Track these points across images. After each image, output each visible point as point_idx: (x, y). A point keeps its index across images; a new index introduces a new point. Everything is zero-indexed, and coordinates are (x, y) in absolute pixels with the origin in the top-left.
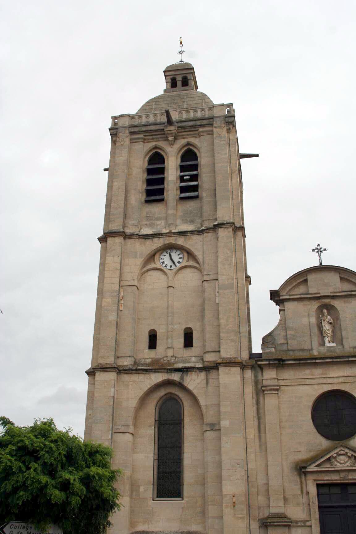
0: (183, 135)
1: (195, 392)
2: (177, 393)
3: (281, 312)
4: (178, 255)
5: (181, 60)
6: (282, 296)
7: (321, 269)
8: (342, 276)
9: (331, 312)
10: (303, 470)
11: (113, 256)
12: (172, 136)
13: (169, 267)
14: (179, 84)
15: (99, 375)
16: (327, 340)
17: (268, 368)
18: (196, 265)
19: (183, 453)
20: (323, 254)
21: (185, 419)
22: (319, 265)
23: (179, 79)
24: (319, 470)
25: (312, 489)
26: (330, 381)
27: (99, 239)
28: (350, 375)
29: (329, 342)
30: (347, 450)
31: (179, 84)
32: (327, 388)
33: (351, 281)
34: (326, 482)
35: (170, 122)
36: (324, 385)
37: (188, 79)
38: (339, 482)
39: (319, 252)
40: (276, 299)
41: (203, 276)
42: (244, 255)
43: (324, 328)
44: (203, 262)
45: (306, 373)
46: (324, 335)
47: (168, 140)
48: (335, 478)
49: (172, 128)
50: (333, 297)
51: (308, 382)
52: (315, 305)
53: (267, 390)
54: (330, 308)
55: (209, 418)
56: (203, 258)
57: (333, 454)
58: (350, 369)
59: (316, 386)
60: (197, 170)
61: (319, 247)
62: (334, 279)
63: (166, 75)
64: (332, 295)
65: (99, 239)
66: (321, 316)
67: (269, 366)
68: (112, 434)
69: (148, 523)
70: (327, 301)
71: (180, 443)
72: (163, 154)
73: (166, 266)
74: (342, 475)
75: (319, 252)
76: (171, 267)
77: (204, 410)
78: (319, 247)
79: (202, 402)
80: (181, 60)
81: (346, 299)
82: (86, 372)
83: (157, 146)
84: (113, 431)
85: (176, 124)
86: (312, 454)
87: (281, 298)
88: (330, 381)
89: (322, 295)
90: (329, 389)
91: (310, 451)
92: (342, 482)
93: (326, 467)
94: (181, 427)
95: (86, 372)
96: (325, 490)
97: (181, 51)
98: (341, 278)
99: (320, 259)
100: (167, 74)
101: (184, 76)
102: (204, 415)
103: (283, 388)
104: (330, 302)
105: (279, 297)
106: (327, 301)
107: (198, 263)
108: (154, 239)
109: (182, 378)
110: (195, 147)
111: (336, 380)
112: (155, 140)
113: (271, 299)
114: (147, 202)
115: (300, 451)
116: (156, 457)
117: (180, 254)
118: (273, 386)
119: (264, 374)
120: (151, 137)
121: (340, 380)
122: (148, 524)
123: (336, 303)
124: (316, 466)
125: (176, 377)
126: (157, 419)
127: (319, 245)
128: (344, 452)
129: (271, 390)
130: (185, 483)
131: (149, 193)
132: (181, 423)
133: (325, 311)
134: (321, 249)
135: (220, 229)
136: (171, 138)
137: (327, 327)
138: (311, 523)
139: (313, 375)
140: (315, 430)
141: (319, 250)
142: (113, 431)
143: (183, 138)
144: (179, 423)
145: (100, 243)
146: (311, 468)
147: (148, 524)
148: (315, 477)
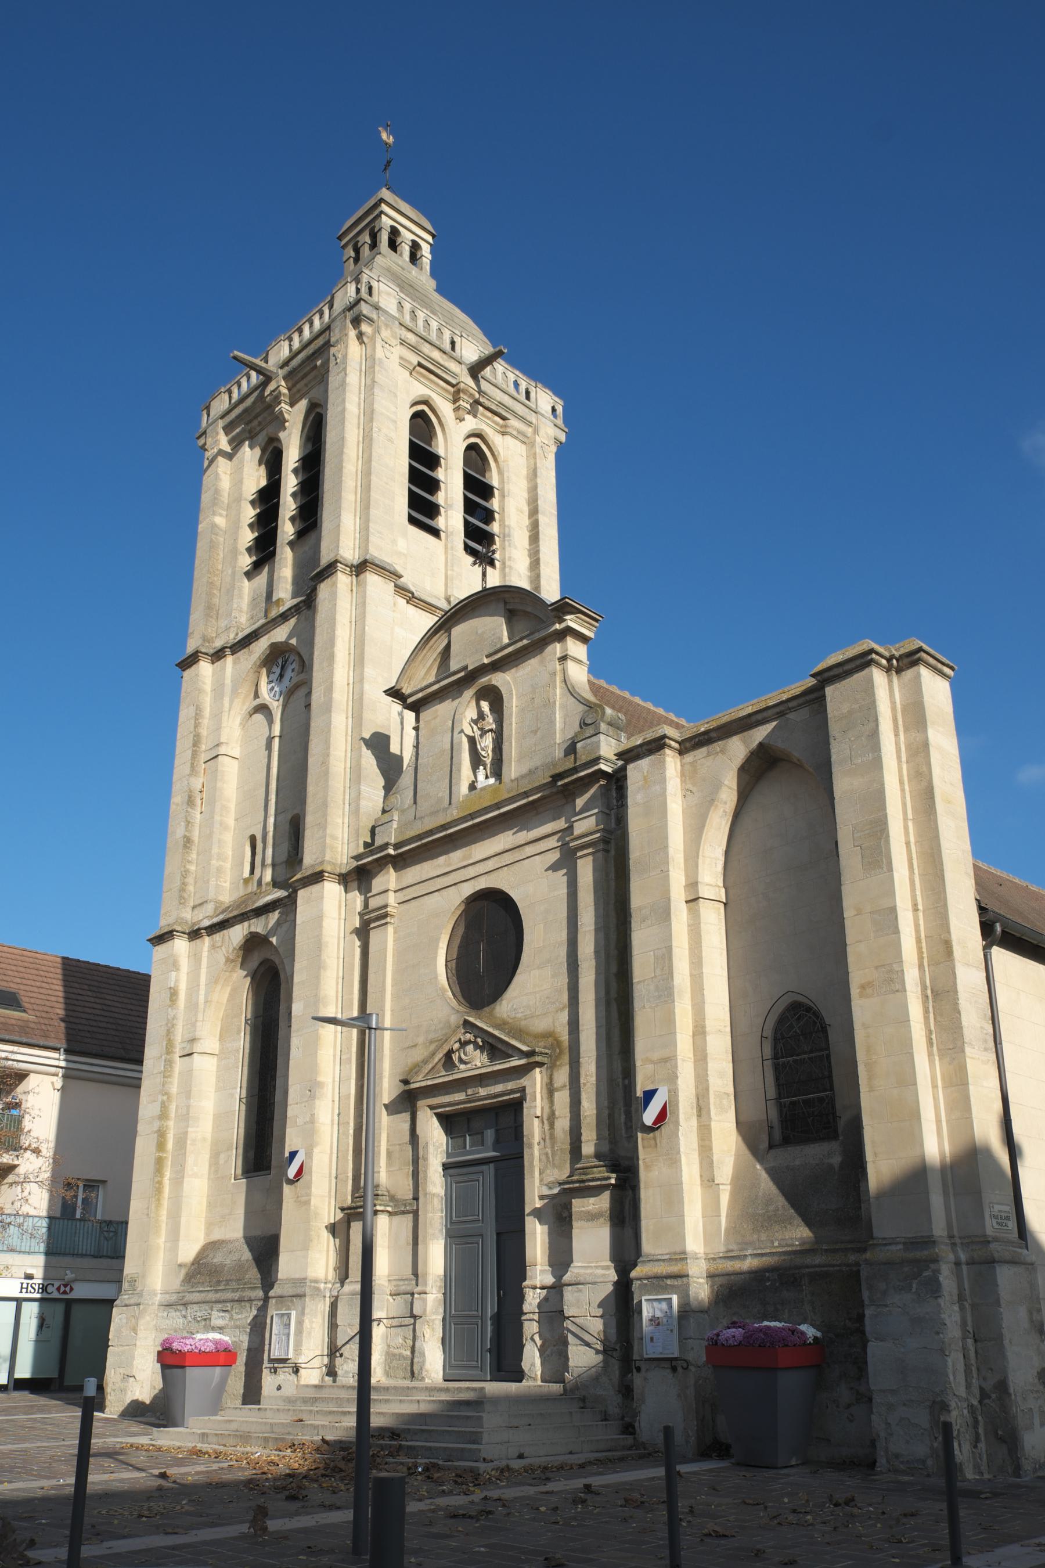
32: (468, 890)
99: (483, 580)
104: (490, 680)
116: (244, 1095)
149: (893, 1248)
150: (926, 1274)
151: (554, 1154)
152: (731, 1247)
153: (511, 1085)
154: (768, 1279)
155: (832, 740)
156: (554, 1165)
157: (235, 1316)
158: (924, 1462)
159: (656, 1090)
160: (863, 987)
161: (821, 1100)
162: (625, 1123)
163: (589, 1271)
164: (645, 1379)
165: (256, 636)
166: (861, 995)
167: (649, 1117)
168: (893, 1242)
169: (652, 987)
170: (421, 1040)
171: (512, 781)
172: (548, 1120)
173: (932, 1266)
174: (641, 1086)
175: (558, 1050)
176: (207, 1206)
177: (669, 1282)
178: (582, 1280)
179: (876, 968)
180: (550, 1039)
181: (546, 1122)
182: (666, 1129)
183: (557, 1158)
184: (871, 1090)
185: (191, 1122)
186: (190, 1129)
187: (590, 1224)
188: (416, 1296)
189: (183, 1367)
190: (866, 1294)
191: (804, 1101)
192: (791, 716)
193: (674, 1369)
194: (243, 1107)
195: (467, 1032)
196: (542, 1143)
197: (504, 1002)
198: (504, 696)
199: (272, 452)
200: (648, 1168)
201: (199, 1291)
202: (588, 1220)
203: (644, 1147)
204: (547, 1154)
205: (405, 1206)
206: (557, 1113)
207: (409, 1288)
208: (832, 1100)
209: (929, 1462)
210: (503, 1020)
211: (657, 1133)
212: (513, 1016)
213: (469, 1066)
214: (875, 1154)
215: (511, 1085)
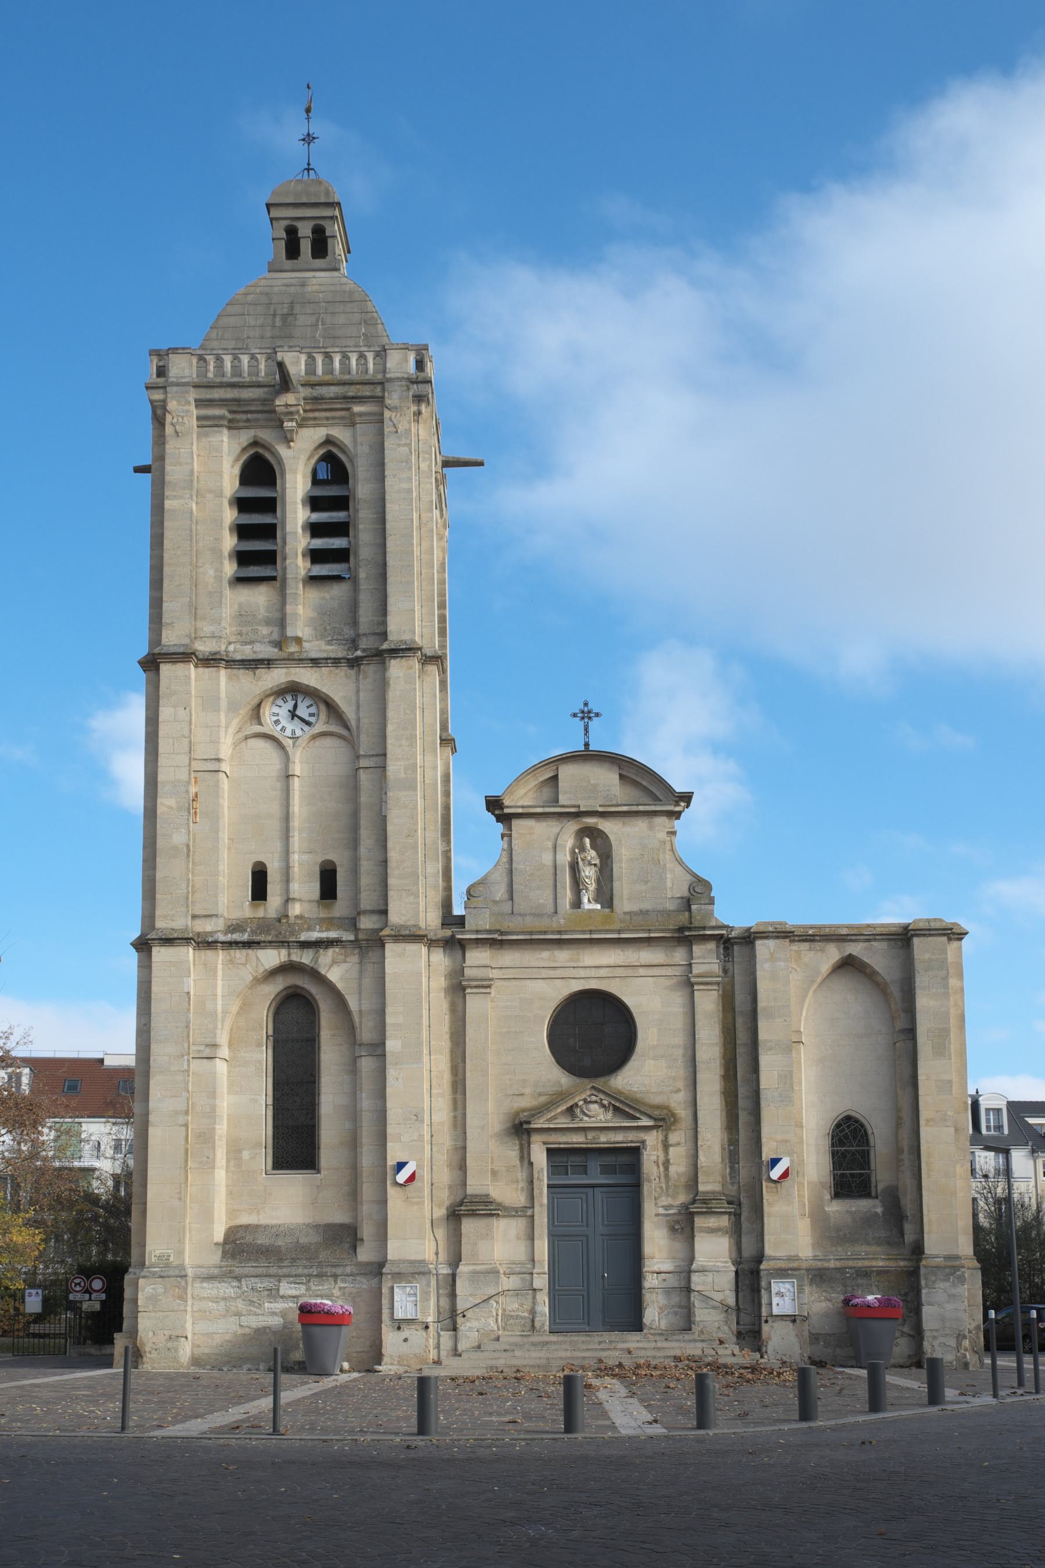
0: (315, 419)
1: (340, 986)
2: (307, 986)
3: (505, 838)
4: (308, 707)
5: (309, 164)
6: (508, 807)
7: (587, 756)
8: (624, 773)
9: (599, 841)
10: (525, 1126)
11: (175, 707)
12: (292, 420)
13: (288, 733)
14: (306, 247)
15: (159, 952)
16: (585, 900)
17: (475, 946)
18: (345, 732)
19: (319, 1094)
20: (594, 724)
21: (322, 1033)
22: (583, 749)
23: (305, 231)
24: (551, 1126)
25: (539, 1157)
26: (582, 973)
27: (140, 663)
28: (620, 964)
29: (589, 901)
30: (601, 1096)
31: (306, 247)
32: (577, 986)
33: (641, 784)
34: (562, 1146)
35: (285, 383)
36: (573, 980)
37: (327, 234)
38: (584, 1146)
39: (586, 720)
40: (497, 812)
41: (358, 757)
42: (441, 691)
43: (583, 874)
44: (358, 727)
45: (543, 957)
46: (581, 887)
47: (281, 426)
48: (577, 1140)
49: (290, 398)
50: (603, 815)
51: (545, 973)
52: (571, 827)
53: (471, 987)
54: (595, 835)
55: (366, 1034)
56: (358, 720)
57: (578, 1099)
58: (622, 953)
59: (558, 982)
60: (346, 508)
61: (586, 709)
62: (607, 778)
63: (271, 216)
64: (600, 809)
65: (140, 663)
66: (577, 851)
67: (477, 943)
68: (188, 1061)
69: (258, 1211)
70: (590, 821)
71: (313, 1076)
72: (269, 440)
73: (283, 729)
74: (591, 1135)
75: (586, 720)
76: (293, 732)
77: (357, 1020)
78: (586, 709)
79: (353, 1004)
80: (309, 164)
81: (627, 820)
82: (131, 944)
83: (259, 440)
84: (191, 1056)
85: (301, 389)
86: (543, 1099)
87: (506, 811)
88: (582, 973)
89: (582, 809)
90: (581, 988)
91: (540, 1095)
92: (589, 1146)
93: (563, 1122)
94: (313, 1047)
95: (131, 944)
96: (561, 1159)
97: (309, 144)
98: (621, 776)
99: (585, 735)
100: (276, 213)
101: (316, 225)
102: (293, 837)
103: (497, 984)
104: (597, 823)
105: (502, 809)
106: (590, 821)
107: (347, 727)
108: (258, 671)
109: (316, 959)
110: (344, 452)
111: (593, 973)
112: (252, 423)
113: (488, 809)
114: (240, 580)
115: (522, 1095)
116: (270, 1101)
117: (311, 705)
118: (482, 980)
119: (468, 955)
120: (244, 417)
121: (602, 972)
122: (258, 1213)
123: (606, 826)
124: (548, 1120)
125: (305, 958)
126: (271, 1032)
127: (586, 704)
128: (597, 1099)
129: (476, 987)
130: (322, 1146)
131: (243, 558)
132: (314, 1040)
133: (587, 841)
134: (589, 712)
135: (393, 662)
136: (290, 424)
137: (589, 874)
138: (533, 1212)
139: (555, 961)
140: (550, 1058)
141: (586, 715)
142: (191, 1056)
143: (319, 426)
144: (311, 1043)
145: (144, 671)
146: (539, 1123)
147: (258, 1213)
148: (546, 1137)
149: (938, 1259)
150: (958, 1273)
151: (667, 1187)
152: (817, 1254)
153: (632, 1136)
154: (848, 1273)
155: (916, 973)
156: (668, 1195)
157: (313, 1287)
158: (951, 1363)
159: (780, 1159)
160: (928, 1121)
161: (861, 1175)
162: (730, 1174)
163: (711, 1264)
164: (772, 1327)
165: (269, 664)
166: (926, 1125)
167: (776, 1173)
168: (937, 1257)
169: (776, 1094)
170: (528, 1091)
171: (625, 913)
172: (663, 1164)
173: (962, 1270)
174: (767, 1154)
175: (672, 1119)
176: (227, 1195)
177: (790, 1272)
178: (708, 1269)
179: (937, 1112)
180: (665, 1111)
181: (661, 1166)
182: (786, 1183)
183: (670, 1190)
184: (929, 1176)
185: (217, 1120)
186: (217, 1126)
187: (708, 1235)
188: (535, 1275)
189: (340, 1325)
190: (923, 1282)
191: (850, 1174)
192: (874, 943)
193: (794, 1321)
194: (270, 1113)
195: (593, 1095)
196: (657, 1179)
197: (619, 1078)
198: (613, 842)
199: (251, 455)
200: (770, 1204)
201: (253, 1267)
202: (709, 1233)
203: (767, 1192)
204: (661, 1188)
205: (517, 1212)
206: (671, 1161)
207: (530, 1271)
208: (869, 1177)
209: (954, 1363)
210: (618, 1090)
211: (779, 1185)
212: (629, 1088)
213: (593, 1119)
214: (929, 1211)
215: (632, 1136)
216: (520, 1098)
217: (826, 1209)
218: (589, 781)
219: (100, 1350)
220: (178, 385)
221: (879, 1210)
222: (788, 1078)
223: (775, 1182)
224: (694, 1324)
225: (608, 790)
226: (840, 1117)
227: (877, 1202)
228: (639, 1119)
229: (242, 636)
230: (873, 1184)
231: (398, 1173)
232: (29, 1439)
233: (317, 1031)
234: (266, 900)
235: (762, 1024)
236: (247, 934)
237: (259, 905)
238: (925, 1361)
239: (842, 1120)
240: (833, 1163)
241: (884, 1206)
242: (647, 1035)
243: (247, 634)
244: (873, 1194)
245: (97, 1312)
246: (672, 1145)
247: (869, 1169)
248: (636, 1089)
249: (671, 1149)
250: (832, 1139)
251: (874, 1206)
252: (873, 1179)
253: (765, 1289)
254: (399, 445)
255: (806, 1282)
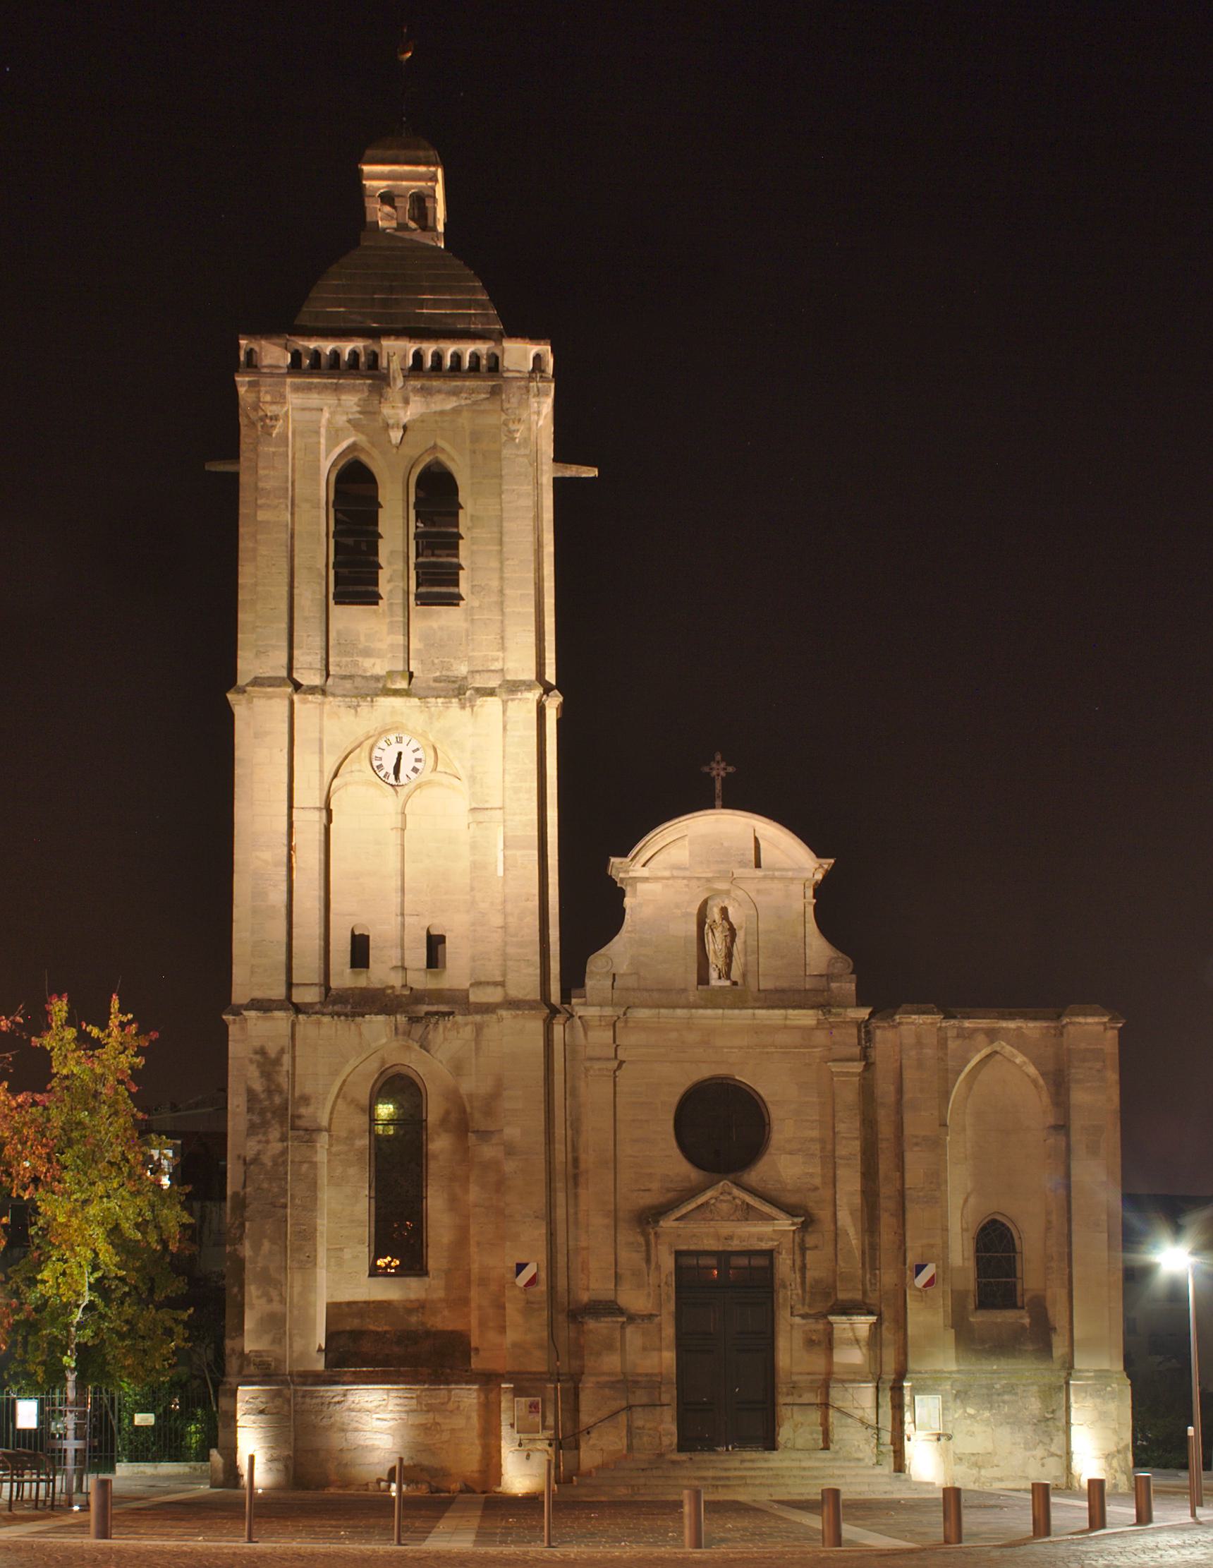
86: (671, 1195)
91: (668, 1190)
115: (649, 1190)
159: (926, 1266)
170: (655, 1186)
181: (797, 1272)
197: (753, 1173)
206: (808, 1266)
216: (647, 1194)
217: (971, 1319)
218: (722, 844)
219: (156, 1467)
220: (272, 375)
221: (1027, 1321)
222: (936, 1178)
223: (919, 1290)
224: (832, 1442)
225: (743, 854)
226: (986, 1220)
227: (1023, 1312)
228: (774, 1219)
229: (341, 667)
230: (1019, 1293)
231: (535, 1274)
232: (214, 1550)
233: (424, 1115)
234: (368, 967)
235: (908, 1117)
236: (349, 1007)
237: (360, 974)
238: (482, 1550)
239: (988, 1223)
240: (978, 1269)
241: (1030, 1317)
242: (783, 1129)
243: (347, 665)
244: (1019, 1304)
245: (152, 1427)
246: (809, 1249)
247: (1015, 1277)
248: (770, 1186)
249: (808, 1252)
250: (977, 1243)
251: (1021, 1318)
252: (1019, 1287)
253: (908, 1406)
254: (517, 456)
255: (950, 1398)
